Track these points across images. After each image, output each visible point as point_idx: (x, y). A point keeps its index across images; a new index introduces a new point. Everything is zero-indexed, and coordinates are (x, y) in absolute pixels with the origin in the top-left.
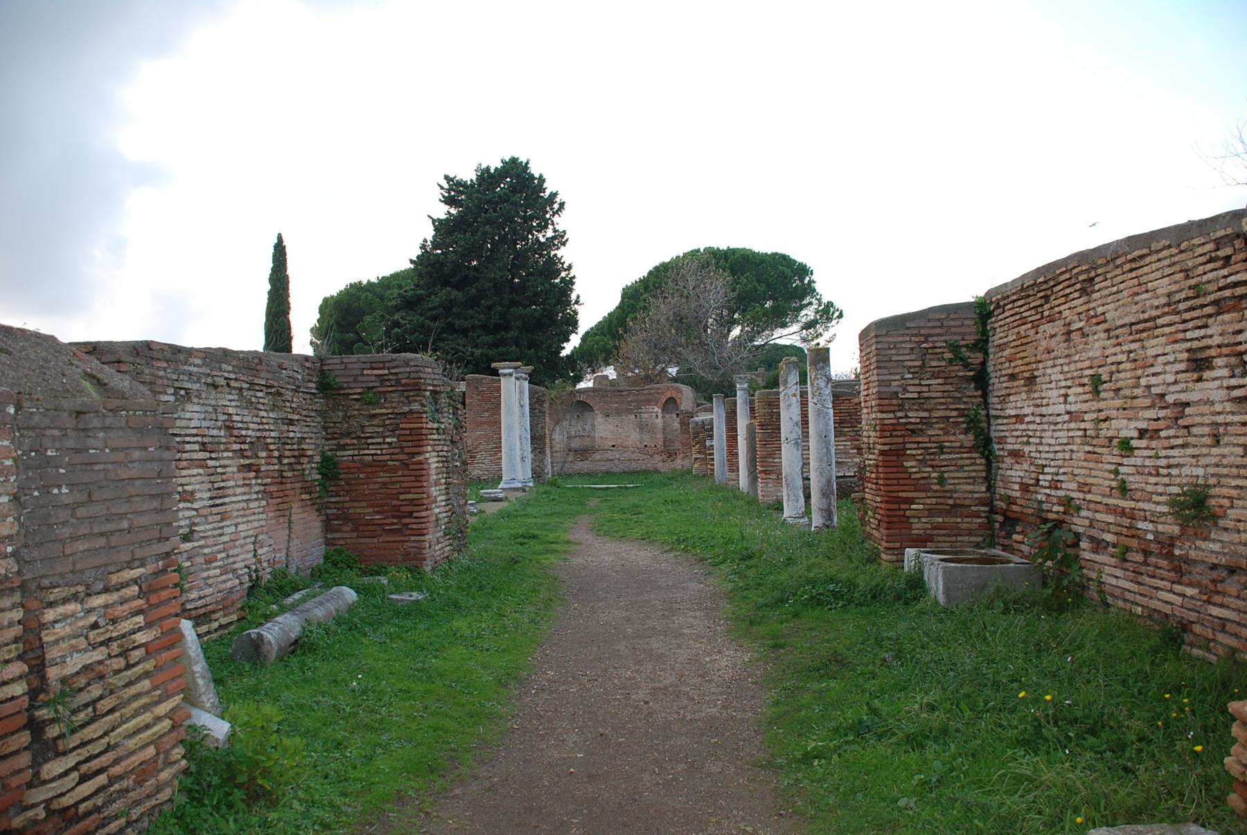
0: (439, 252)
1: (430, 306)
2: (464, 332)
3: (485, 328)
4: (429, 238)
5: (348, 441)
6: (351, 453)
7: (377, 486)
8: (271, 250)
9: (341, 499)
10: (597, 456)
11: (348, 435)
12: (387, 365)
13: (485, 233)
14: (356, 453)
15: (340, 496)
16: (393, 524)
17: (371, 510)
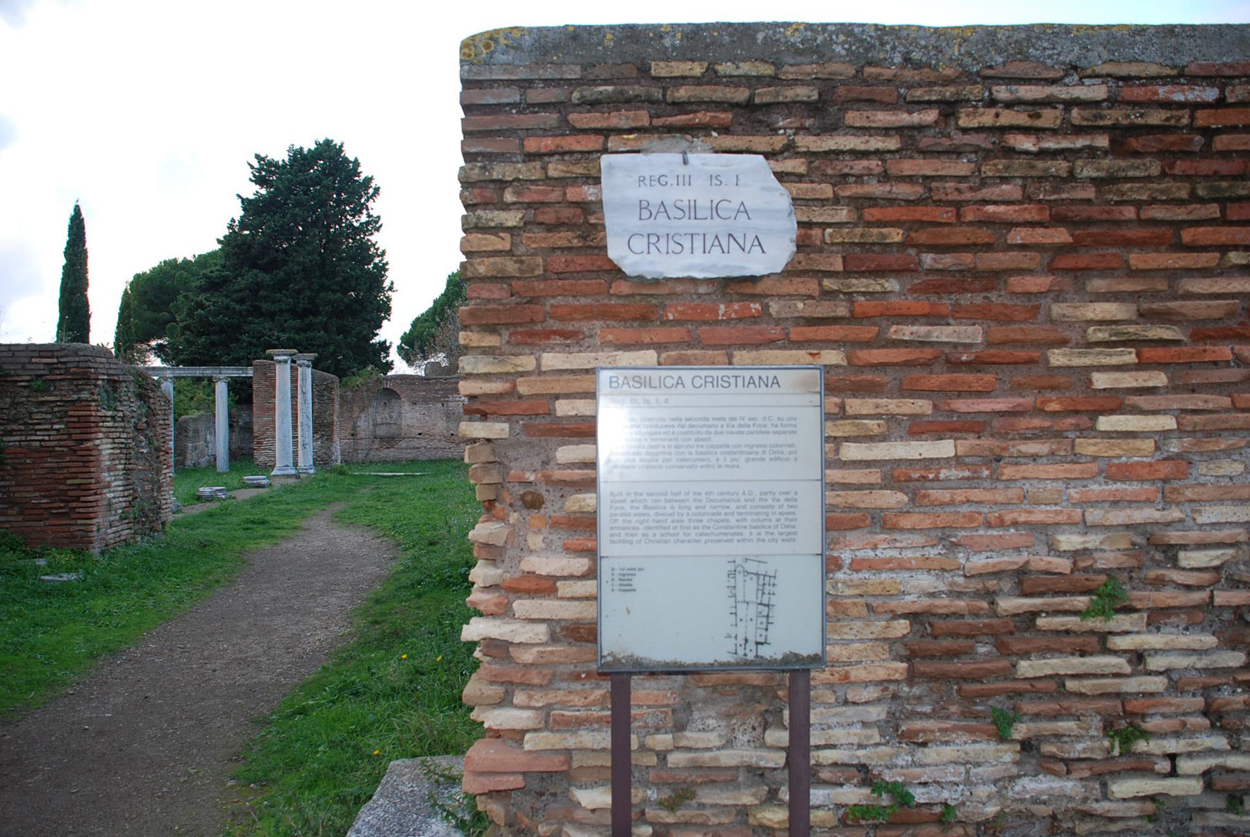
0: (247, 232)
1: (236, 287)
2: (271, 315)
3: (294, 313)
4: (237, 218)
5: (15, 427)
6: (17, 438)
7: (44, 471)
8: (67, 222)
9: (7, 483)
10: (403, 444)
11: (15, 421)
12: (55, 354)
13: (294, 216)
14: (23, 438)
15: (5, 480)
16: (60, 508)
17: (38, 494)
